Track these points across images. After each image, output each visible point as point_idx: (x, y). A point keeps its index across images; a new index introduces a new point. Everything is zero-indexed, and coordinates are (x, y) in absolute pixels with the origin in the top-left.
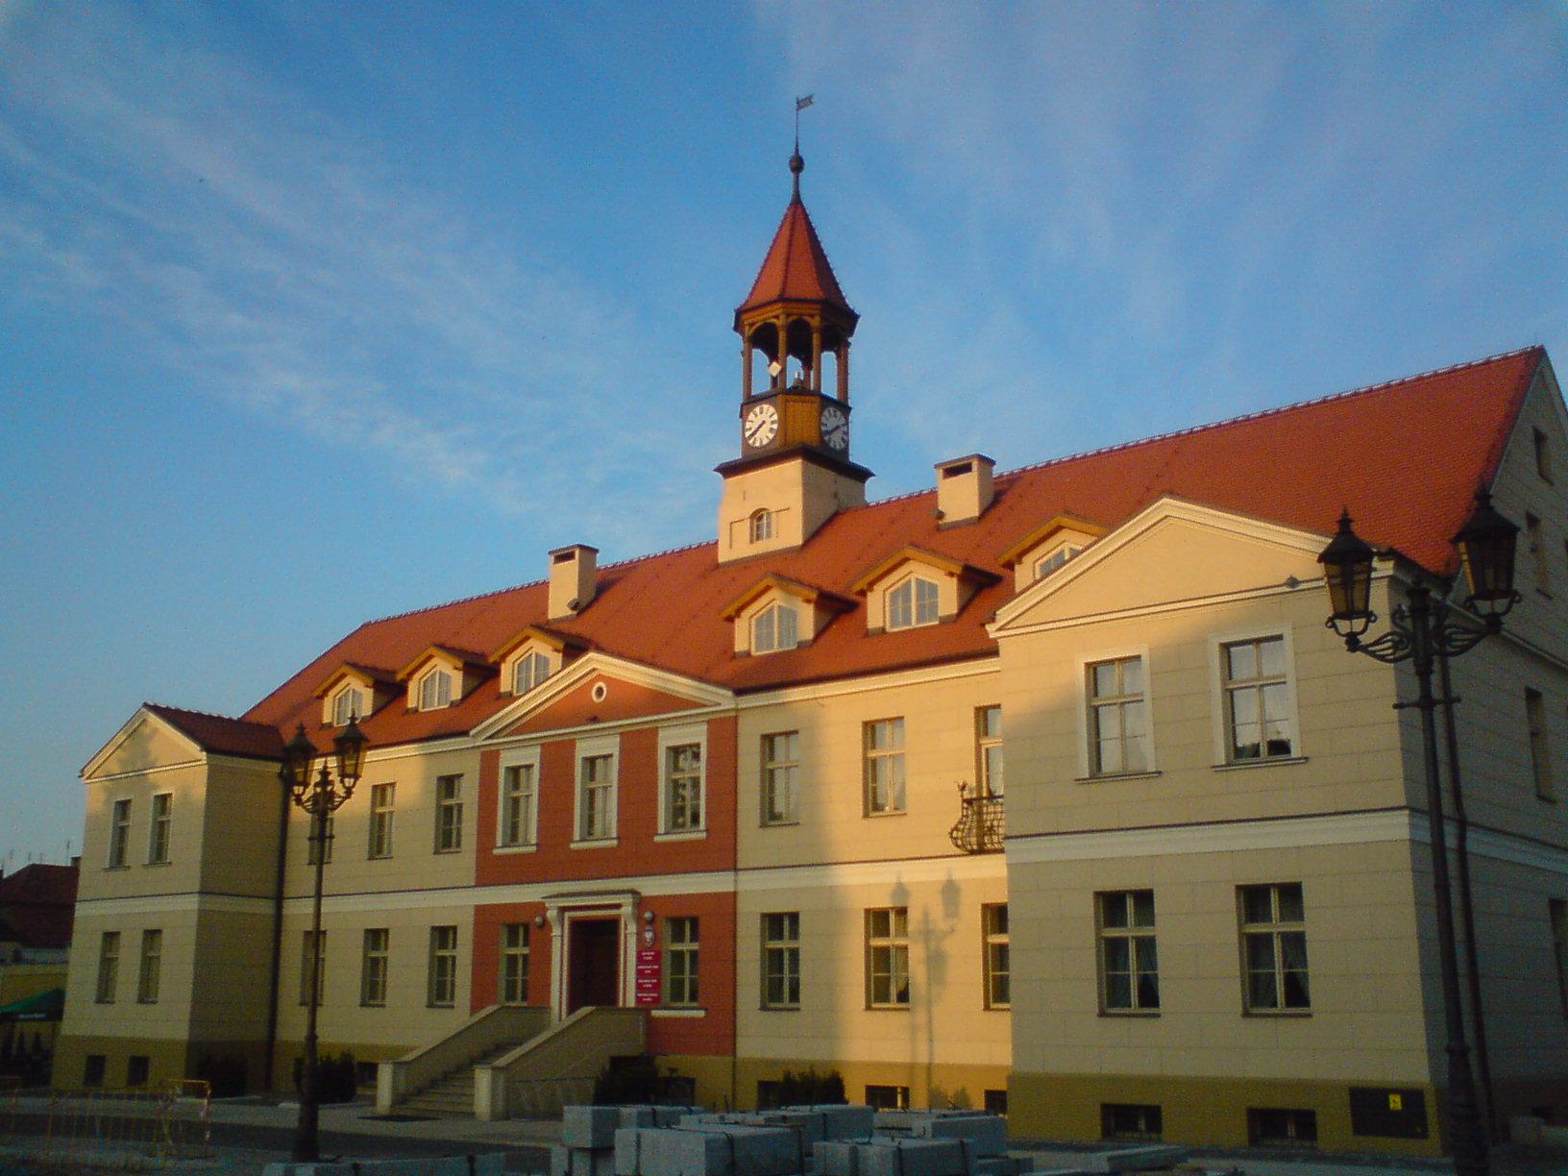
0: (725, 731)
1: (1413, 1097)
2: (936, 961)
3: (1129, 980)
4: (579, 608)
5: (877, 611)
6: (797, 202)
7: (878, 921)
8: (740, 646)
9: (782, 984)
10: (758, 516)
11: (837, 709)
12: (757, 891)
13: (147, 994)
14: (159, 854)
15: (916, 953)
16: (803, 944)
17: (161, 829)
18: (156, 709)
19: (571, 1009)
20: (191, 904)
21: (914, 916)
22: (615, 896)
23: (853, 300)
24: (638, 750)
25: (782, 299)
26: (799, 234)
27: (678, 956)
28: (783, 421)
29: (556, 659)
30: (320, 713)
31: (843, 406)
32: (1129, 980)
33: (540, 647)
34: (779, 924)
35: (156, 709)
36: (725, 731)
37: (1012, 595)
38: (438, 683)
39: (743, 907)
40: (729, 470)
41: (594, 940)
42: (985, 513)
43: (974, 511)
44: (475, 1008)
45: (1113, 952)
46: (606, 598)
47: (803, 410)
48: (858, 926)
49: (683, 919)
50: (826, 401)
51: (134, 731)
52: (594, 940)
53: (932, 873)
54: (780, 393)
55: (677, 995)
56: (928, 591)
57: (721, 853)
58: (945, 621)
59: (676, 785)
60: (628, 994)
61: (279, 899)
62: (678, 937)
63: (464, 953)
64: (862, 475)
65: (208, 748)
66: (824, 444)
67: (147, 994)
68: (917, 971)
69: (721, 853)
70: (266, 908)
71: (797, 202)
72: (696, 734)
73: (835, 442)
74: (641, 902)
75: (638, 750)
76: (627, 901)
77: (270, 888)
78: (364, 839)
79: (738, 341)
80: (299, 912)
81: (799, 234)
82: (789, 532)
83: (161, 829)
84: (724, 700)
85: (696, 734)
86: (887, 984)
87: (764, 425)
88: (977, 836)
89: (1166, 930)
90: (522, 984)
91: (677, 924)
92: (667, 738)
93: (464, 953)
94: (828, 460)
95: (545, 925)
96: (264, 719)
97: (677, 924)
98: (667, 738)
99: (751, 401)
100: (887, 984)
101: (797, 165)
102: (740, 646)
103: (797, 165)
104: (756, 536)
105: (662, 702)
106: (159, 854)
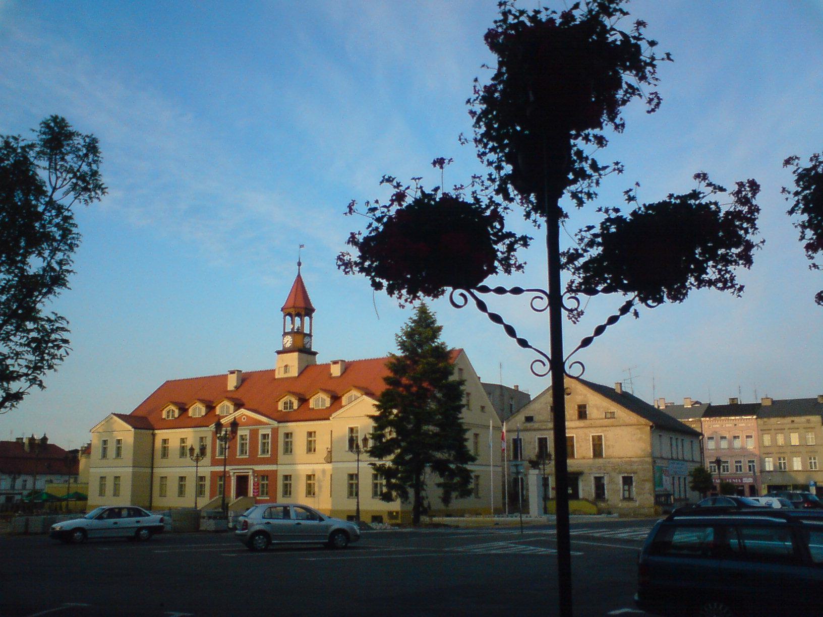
0: (275, 431)
1: (397, 513)
2: (320, 487)
3: (353, 491)
4: (237, 388)
5: (312, 404)
6: (299, 280)
7: (309, 477)
8: (280, 409)
9: (287, 491)
10: (286, 366)
11: (299, 430)
12: (282, 470)
13: (116, 493)
14: (118, 454)
15: (316, 485)
16: (293, 482)
17: (119, 449)
18: (120, 416)
19: (237, 497)
20: (131, 469)
21: (316, 477)
22: (248, 470)
23: (314, 304)
24: (254, 433)
25: (294, 307)
26: (299, 287)
27: (263, 485)
28: (294, 341)
29: (232, 408)
30: (161, 415)
31: (310, 335)
32: (353, 491)
33: (227, 403)
34: (287, 477)
35: (120, 416)
36: (275, 431)
37: (342, 407)
38: (197, 410)
39: (279, 473)
40: (279, 352)
41: (242, 481)
42: (342, 375)
43: (339, 374)
44: (211, 497)
45: (351, 485)
46: (245, 384)
47: (300, 337)
48: (304, 478)
49: (264, 476)
50: (306, 335)
51: (108, 420)
52: (242, 481)
53: (321, 467)
54: (293, 333)
55: (263, 494)
56: (323, 400)
57: (273, 460)
58: (327, 408)
59: (264, 444)
60: (251, 494)
61: (152, 468)
62: (263, 480)
63: (208, 483)
64: (315, 354)
65: (135, 428)
66: (304, 347)
67: (116, 493)
68: (316, 490)
69: (273, 460)
70: (149, 470)
71: (299, 280)
72: (269, 431)
73: (308, 346)
74: (254, 472)
75: (254, 433)
76: (251, 471)
77: (149, 465)
78: (178, 453)
79: (282, 314)
80: (159, 472)
81: (299, 287)
82: (294, 372)
83: (119, 449)
84: (275, 424)
85: (269, 431)
86: (310, 492)
87: (288, 341)
88: (329, 460)
89: (168, 483)
90: (224, 491)
91: (263, 477)
92: (261, 432)
93: (208, 483)
94: (305, 350)
95: (230, 476)
96: (140, 413)
97: (263, 477)
98: (261, 432)
99: (285, 334)
100: (310, 492)
101: (299, 264)
102: (280, 409)
103: (299, 264)
104: (286, 372)
105: (260, 423)
106: (118, 454)
